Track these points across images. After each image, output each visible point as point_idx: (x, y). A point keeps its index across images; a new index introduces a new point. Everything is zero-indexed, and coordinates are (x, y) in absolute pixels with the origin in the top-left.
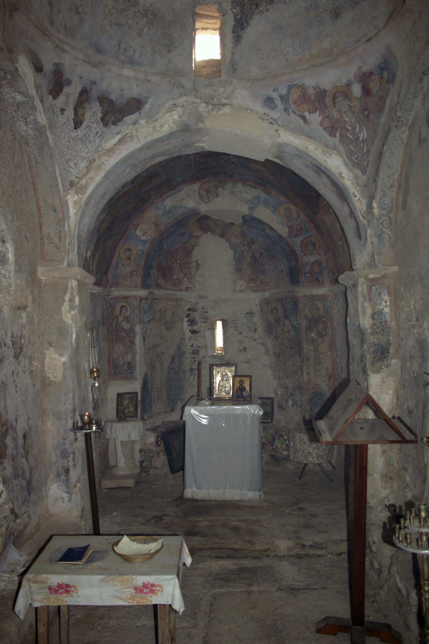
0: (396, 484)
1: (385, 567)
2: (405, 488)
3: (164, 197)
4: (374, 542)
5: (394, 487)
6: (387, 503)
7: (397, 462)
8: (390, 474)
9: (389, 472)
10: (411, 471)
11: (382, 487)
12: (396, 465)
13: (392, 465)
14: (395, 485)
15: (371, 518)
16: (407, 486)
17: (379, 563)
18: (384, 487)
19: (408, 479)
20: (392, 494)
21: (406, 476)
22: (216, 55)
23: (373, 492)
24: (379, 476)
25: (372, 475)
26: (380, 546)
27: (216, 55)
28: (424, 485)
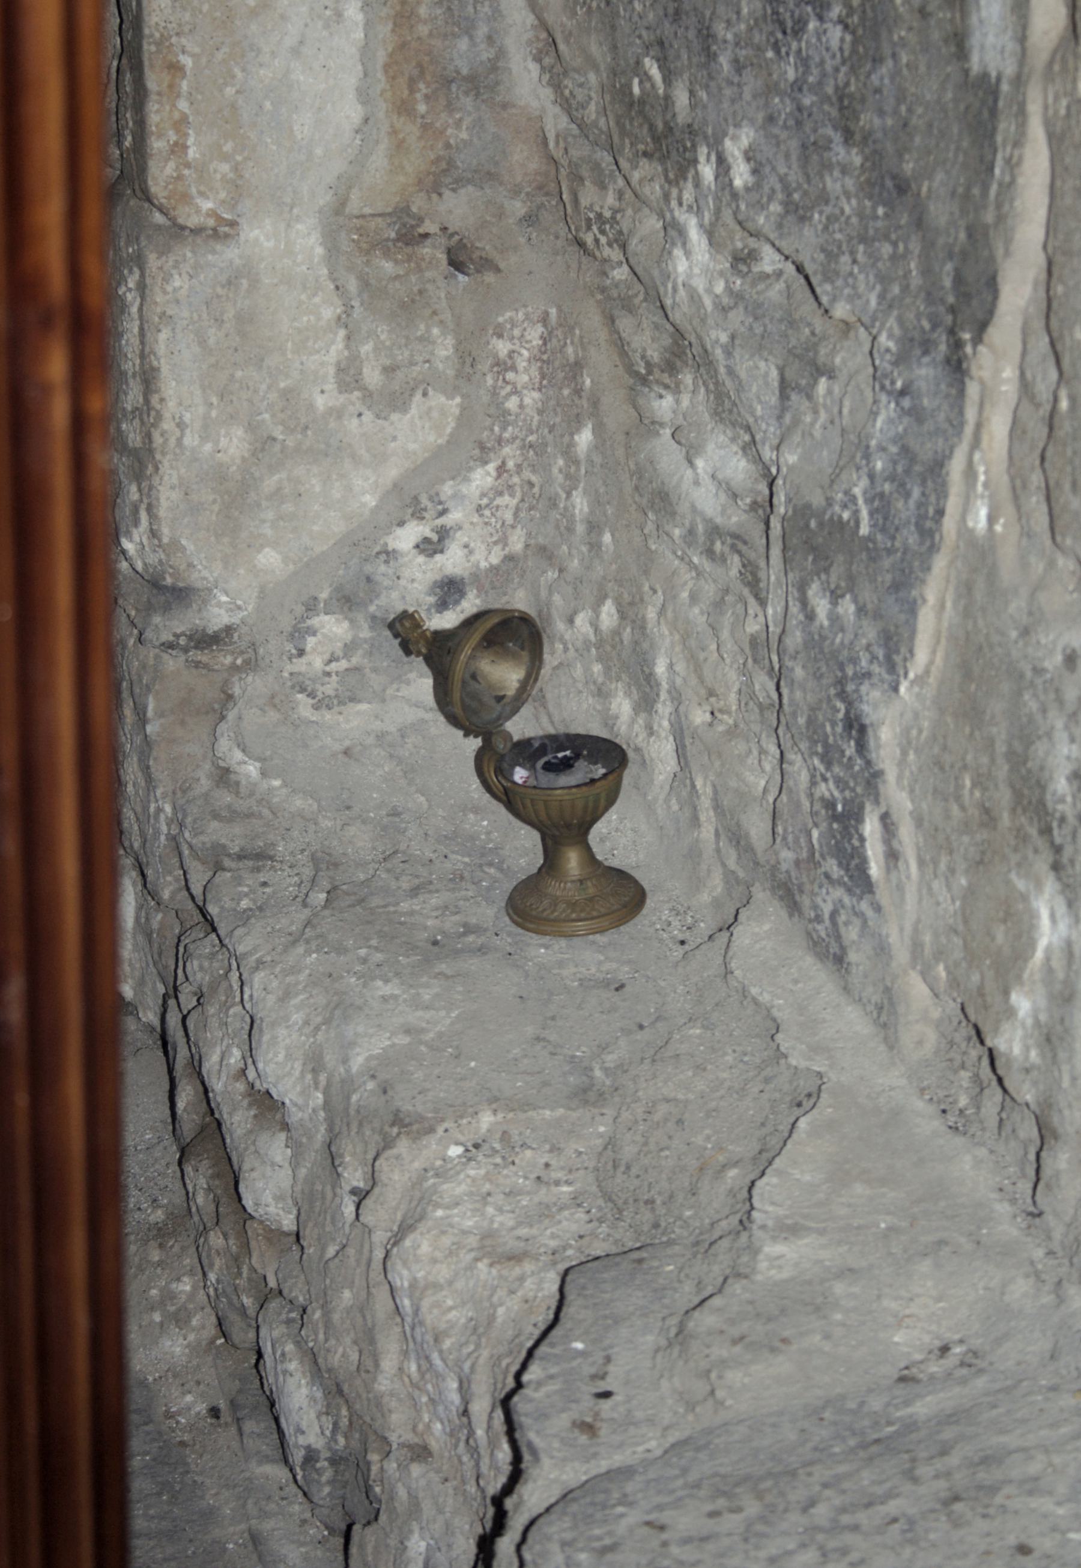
0: (535, 334)
1: (421, 1453)
2: (640, 379)
3: (1021, 906)
4: (266, 1105)
5: (502, 366)
6: (411, 584)
7: (548, 46)
8: (457, 209)
9: (440, 177)
10: (741, 175)
11: (348, 376)
12: (527, 84)
13: (484, 83)
14: (520, 341)
15: (224, 776)
16: (682, 352)
17: (335, 1391)
18: (372, 376)
19: (695, 266)
20: (484, 452)
21: (674, 231)
22: (518, 769)
23: (234, 444)
24: (308, 240)
25: (222, 231)
26: (354, 1177)
27: (518, 769)
28: (957, 367)
